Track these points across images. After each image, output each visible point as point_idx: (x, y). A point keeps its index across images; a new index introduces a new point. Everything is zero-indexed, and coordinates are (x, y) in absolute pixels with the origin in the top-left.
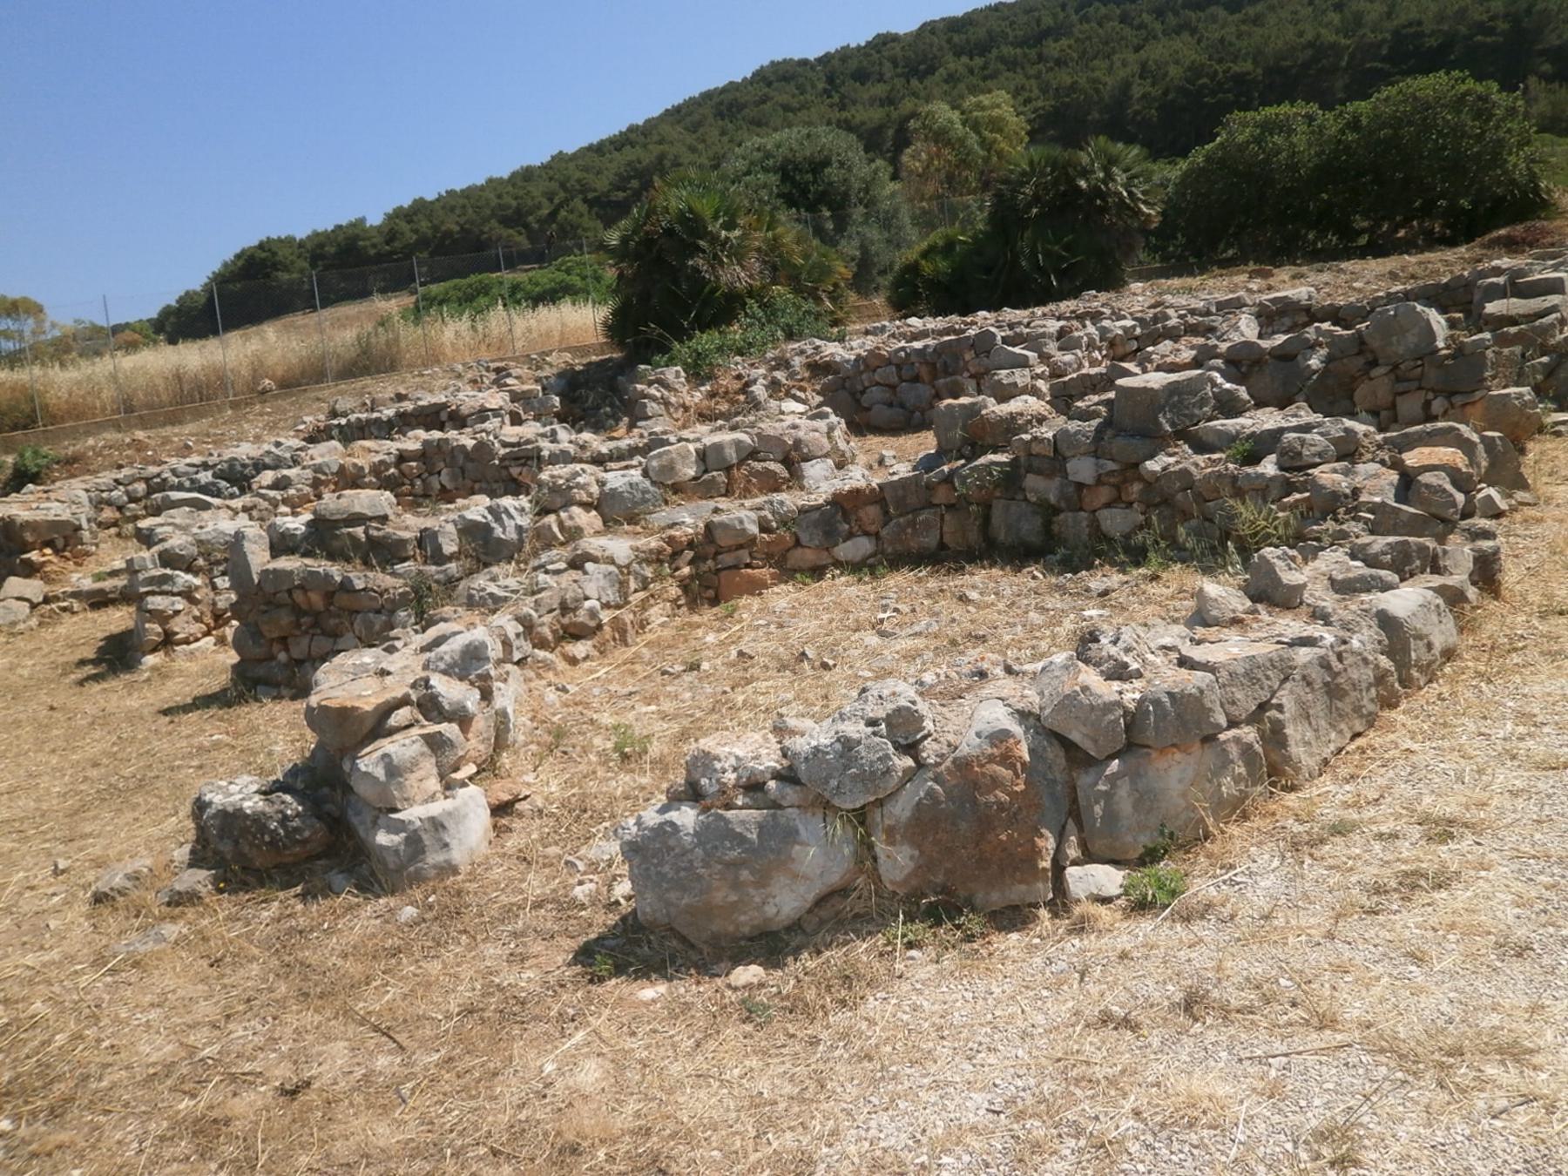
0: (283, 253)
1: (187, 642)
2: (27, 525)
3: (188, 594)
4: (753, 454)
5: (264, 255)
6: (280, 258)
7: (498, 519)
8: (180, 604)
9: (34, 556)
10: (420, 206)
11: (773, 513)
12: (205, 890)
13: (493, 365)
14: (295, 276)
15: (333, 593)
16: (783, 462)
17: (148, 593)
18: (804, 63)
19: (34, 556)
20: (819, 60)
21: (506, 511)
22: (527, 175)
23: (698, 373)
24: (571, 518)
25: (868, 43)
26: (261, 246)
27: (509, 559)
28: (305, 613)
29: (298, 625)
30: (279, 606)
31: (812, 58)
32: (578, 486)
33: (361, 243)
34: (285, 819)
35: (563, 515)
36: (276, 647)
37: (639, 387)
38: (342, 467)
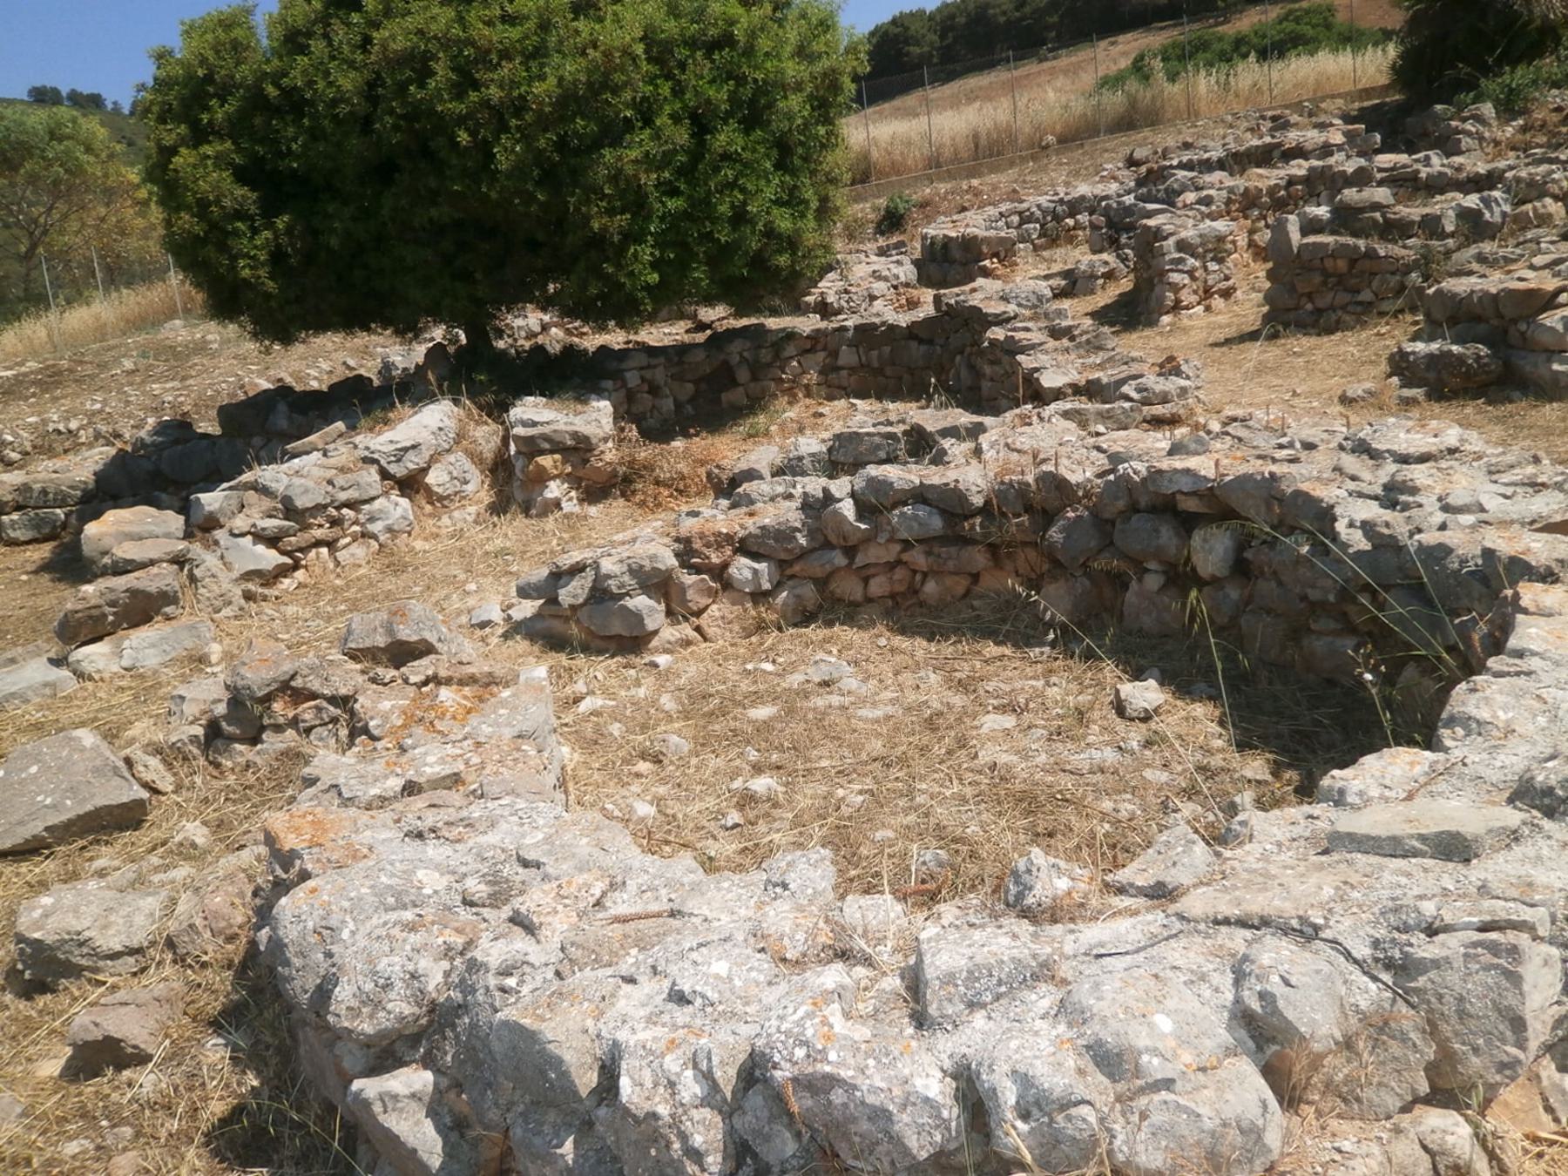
0: (915, 28)
1: (1187, 308)
2: (986, 240)
3: (1191, 273)
5: (897, 30)
6: (912, 31)
7: (1489, 207)
9: (987, 263)
12: (1421, 398)
13: (1270, 114)
14: (926, 49)
15: (1356, 260)
17: (1172, 270)
19: (987, 263)
23: (1509, 107)
24: (1544, 206)
26: (894, 22)
27: (1493, 238)
28: (1331, 275)
29: (1325, 283)
30: (1311, 270)
32: (1554, 181)
33: (991, 11)
34: (1478, 358)
35: (1538, 204)
36: (1304, 300)
37: (1454, 123)
38: (1246, 189)
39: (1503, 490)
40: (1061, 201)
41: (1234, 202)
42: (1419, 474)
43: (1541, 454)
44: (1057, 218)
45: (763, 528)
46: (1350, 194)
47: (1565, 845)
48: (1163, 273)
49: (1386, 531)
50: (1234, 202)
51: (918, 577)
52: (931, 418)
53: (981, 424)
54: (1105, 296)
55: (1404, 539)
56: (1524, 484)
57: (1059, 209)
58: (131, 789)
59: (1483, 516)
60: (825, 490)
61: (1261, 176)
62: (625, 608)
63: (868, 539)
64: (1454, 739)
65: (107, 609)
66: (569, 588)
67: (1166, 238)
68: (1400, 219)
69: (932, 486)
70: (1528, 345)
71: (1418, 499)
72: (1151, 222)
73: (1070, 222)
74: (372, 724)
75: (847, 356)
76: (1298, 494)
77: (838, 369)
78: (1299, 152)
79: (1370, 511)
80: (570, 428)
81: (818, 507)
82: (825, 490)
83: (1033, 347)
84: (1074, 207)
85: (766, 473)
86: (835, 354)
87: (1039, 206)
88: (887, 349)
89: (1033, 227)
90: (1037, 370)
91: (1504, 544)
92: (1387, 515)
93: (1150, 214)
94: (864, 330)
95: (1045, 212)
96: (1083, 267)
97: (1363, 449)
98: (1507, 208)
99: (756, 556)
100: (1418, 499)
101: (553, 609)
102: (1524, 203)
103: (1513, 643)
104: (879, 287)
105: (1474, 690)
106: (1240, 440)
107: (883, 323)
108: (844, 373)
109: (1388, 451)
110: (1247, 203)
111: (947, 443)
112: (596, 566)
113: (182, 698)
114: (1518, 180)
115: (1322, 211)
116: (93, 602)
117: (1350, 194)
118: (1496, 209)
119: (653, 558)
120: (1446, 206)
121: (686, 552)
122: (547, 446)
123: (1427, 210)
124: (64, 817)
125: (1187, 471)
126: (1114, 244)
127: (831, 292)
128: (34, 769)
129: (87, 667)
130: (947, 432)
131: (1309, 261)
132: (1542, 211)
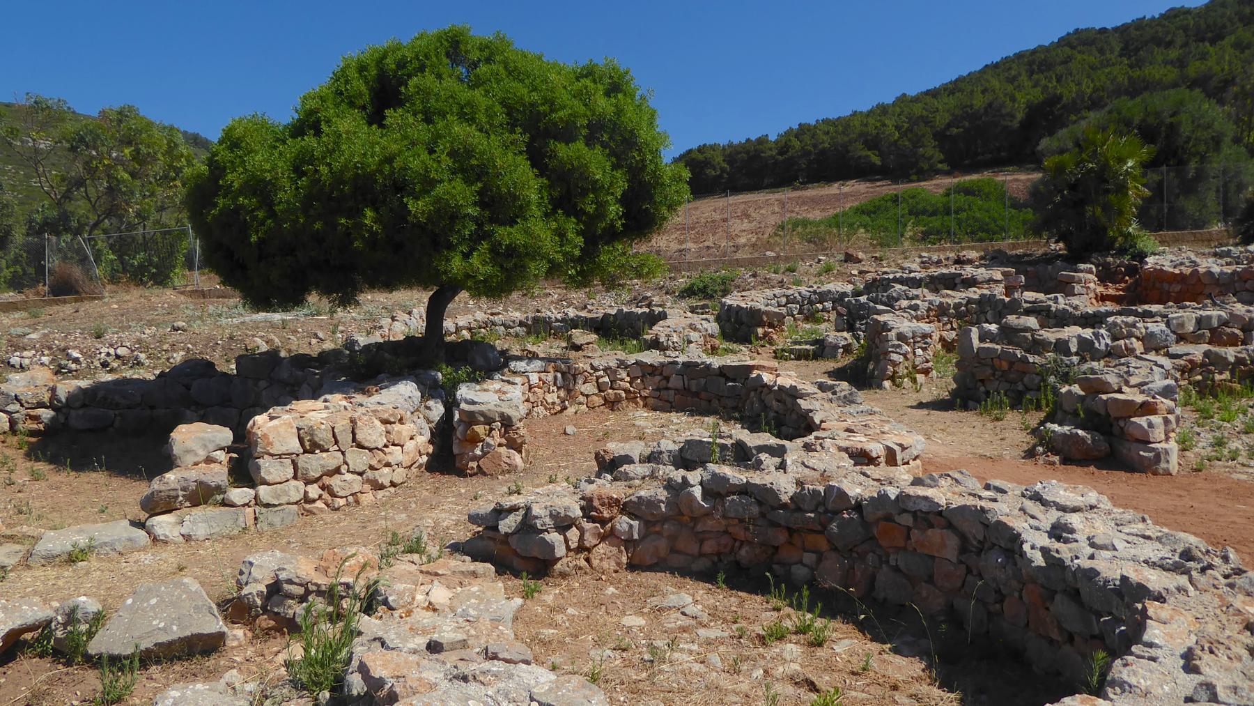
2: (767, 313)
3: (905, 355)
4: (1226, 323)
8: (901, 359)
10: (803, 129)
11: (1249, 355)
16: (1241, 330)
17: (893, 352)
18: (1103, 31)
20: (1116, 29)
21: (1102, 336)
22: (883, 110)
25: (1162, 16)
29: (994, 375)
31: (1109, 27)
39: (1126, 538)
40: (815, 292)
41: (932, 310)
42: (1075, 520)
43: (1146, 516)
44: (811, 303)
45: (640, 498)
46: (1012, 319)
47: (251, 704)
48: (887, 353)
49: (1056, 555)
50: (932, 310)
51: (737, 544)
52: (753, 440)
53: (784, 446)
54: (843, 361)
55: (1068, 562)
56: (1137, 535)
57: (813, 297)
58: (218, 624)
59: (1115, 553)
60: (684, 478)
61: (948, 295)
62: (544, 539)
63: (708, 514)
64: (1115, 694)
65: (181, 493)
66: (507, 521)
67: (890, 330)
68: (1044, 340)
69: (755, 485)
70: (1123, 435)
71: (1075, 536)
72: (881, 318)
73: (820, 306)
74: (390, 599)
75: (675, 382)
76: (999, 523)
77: (667, 389)
78: (971, 282)
79: (1044, 541)
80: (499, 409)
81: (677, 489)
82: (684, 478)
83: (808, 395)
84: (823, 297)
85: (636, 459)
86: (667, 379)
87: (800, 293)
88: (703, 381)
89: (795, 307)
90: (811, 411)
91: (1136, 574)
92: (1057, 545)
93: (879, 313)
94: (688, 366)
95: (803, 298)
96: (830, 340)
97: (1037, 498)
98: (1109, 342)
99: (632, 516)
100: (1075, 536)
101: (491, 534)
102: (1118, 339)
103: (1146, 638)
104: (694, 336)
105: (1126, 665)
106: (956, 480)
107: (703, 363)
108: (672, 392)
109: (1054, 502)
110: (941, 312)
111: (764, 456)
112: (528, 509)
113: (251, 564)
114: (1115, 324)
115: (993, 327)
116: (173, 486)
117: (1012, 319)
118: (1103, 342)
119: (567, 509)
120: (1071, 333)
121: (588, 508)
122: (482, 419)
123: (1059, 336)
124: (170, 638)
125: (926, 498)
126: (851, 328)
127: (663, 335)
128: (153, 601)
129: (159, 531)
130: (761, 449)
131: (982, 358)
132: (1130, 346)
